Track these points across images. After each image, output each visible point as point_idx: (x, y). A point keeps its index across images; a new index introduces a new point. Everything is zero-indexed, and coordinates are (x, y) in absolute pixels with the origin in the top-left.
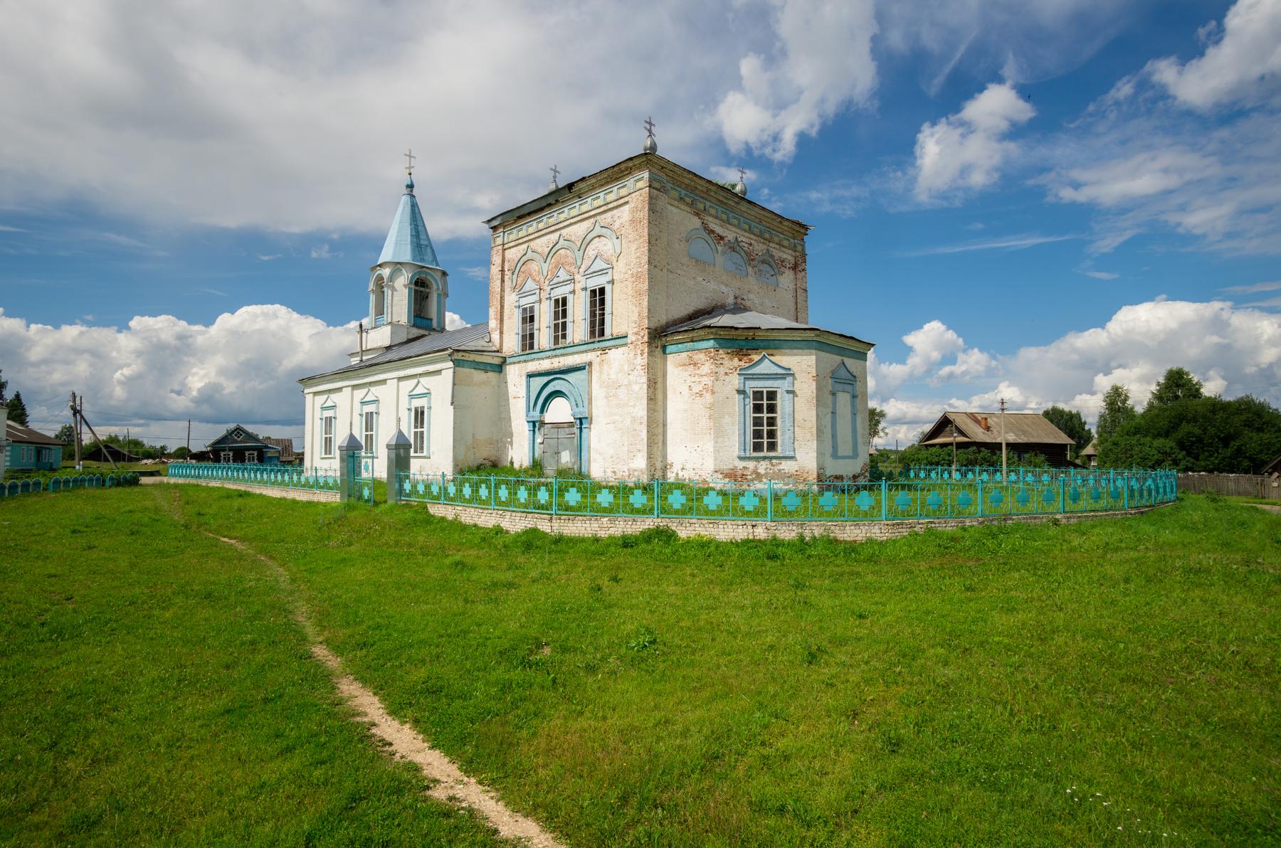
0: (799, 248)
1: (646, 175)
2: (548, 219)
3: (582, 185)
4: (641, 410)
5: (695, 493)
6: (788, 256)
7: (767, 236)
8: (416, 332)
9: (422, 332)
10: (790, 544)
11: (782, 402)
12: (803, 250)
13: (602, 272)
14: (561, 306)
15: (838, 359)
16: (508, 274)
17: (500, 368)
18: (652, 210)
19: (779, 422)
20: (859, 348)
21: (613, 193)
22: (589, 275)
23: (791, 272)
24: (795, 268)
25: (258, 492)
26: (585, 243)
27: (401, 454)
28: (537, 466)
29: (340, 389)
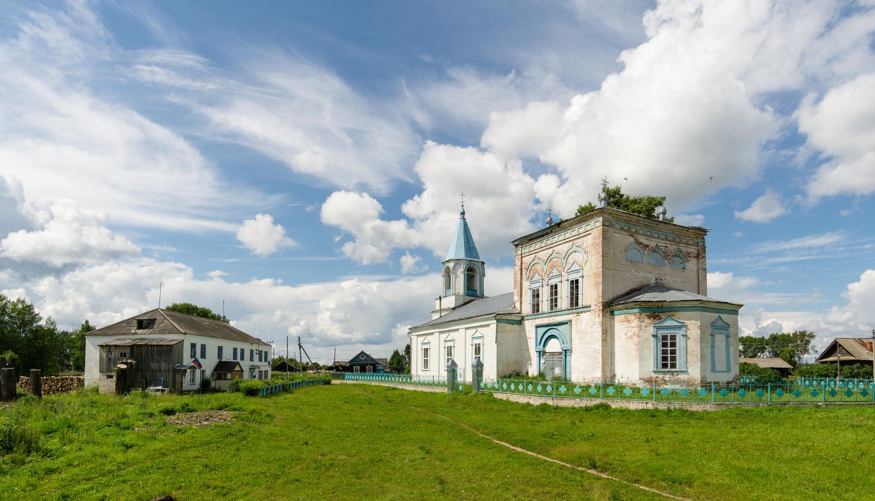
0: (701, 244)
1: (601, 219)
2: (545, 242)
3: (565, 224)
4: (598, 346)
5: (620, 388)
6: (693, 250)
7: (678, 240)
8: (468, 298)
9: (472, 298)
10: (663, 411)
11: (680, 342)
12: (704, 245)
13: (577, 271)
14: (554, 289)
15: (716, 315)
16: (524, 271)
17: (520, 322)
18: (604, 238)
19: (677, 352)
20: (733, 308)
21: (582, 228)
22: (569, 273)
23: (695, 259)
24: (697, 256)
25: (400, 387)
26: (567, 255)
27: (478, 369)
28: (542, 375)
29: (433, 333)
